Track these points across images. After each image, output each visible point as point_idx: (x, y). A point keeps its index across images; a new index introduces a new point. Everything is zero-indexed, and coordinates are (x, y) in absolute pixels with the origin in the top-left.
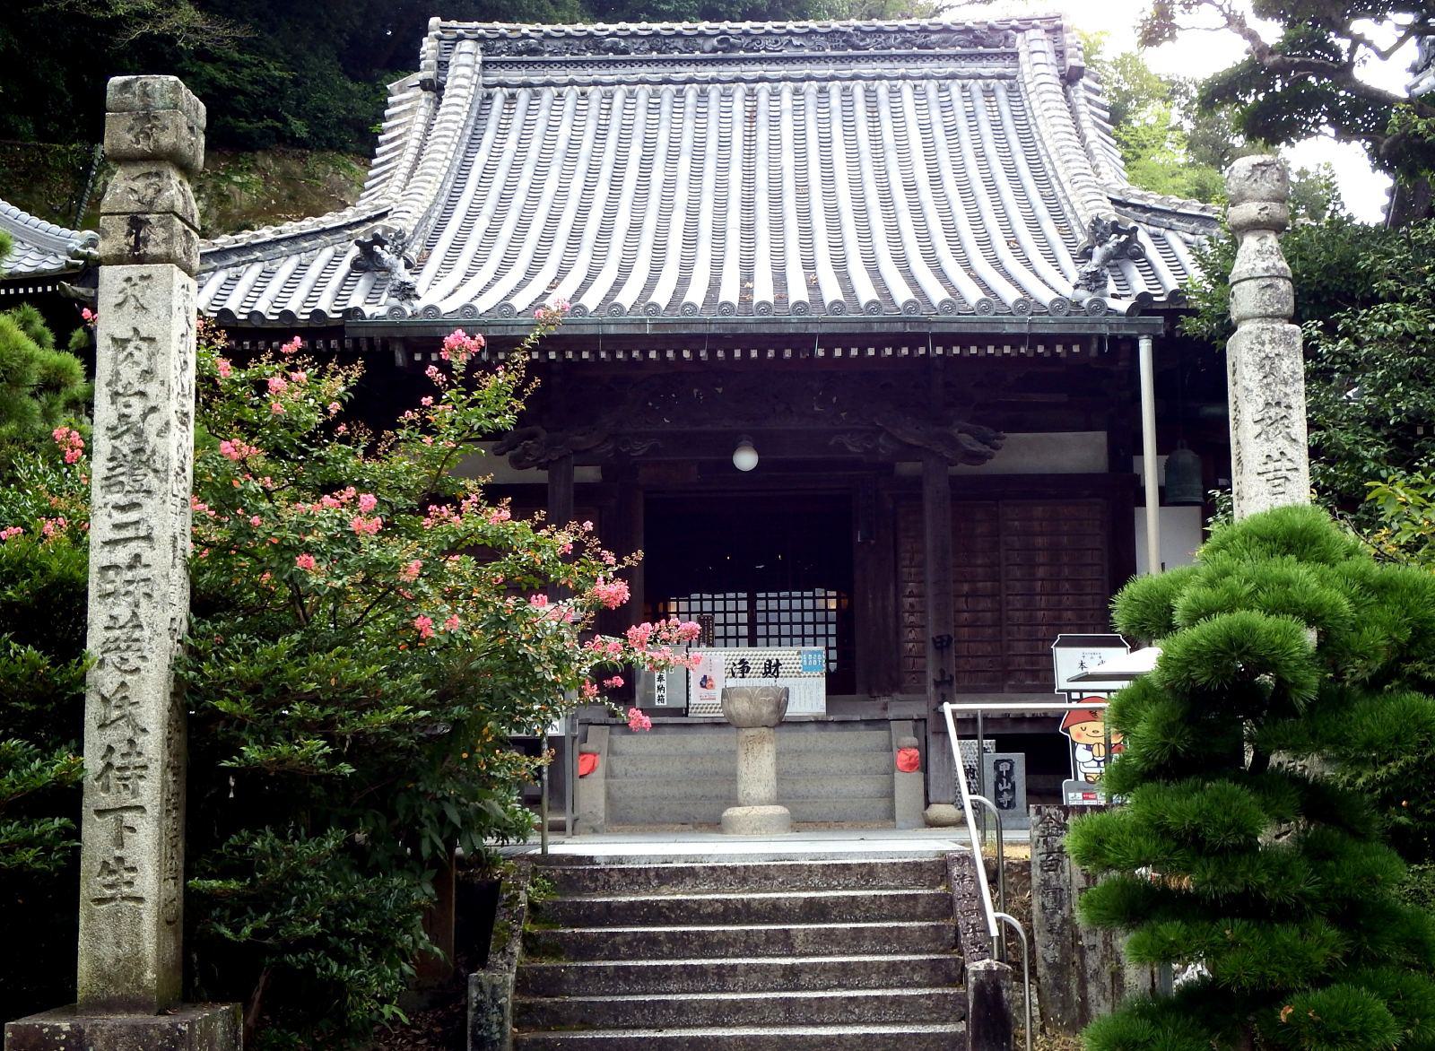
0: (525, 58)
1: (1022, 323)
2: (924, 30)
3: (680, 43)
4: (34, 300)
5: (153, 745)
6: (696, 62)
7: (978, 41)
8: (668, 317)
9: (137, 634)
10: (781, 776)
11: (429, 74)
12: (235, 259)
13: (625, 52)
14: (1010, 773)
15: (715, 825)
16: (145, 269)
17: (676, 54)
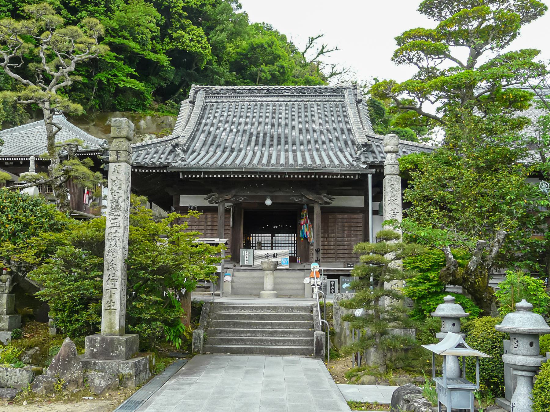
0: (216, 95)
1: (338, 170)
2: (320, 88)
3: (256, 91)
4: (90, 157)
5: (119, 274)
6: (260, 96)
7: (334, 92)
8: (249, 167)
9: (116, 248)
10: (275, 284)
11: (191, 99)
12: (141, 149)
13: (242, 94)
14: (334, 284)
15: (258, 295)
16: (119, 164)
17: (255, 94)
